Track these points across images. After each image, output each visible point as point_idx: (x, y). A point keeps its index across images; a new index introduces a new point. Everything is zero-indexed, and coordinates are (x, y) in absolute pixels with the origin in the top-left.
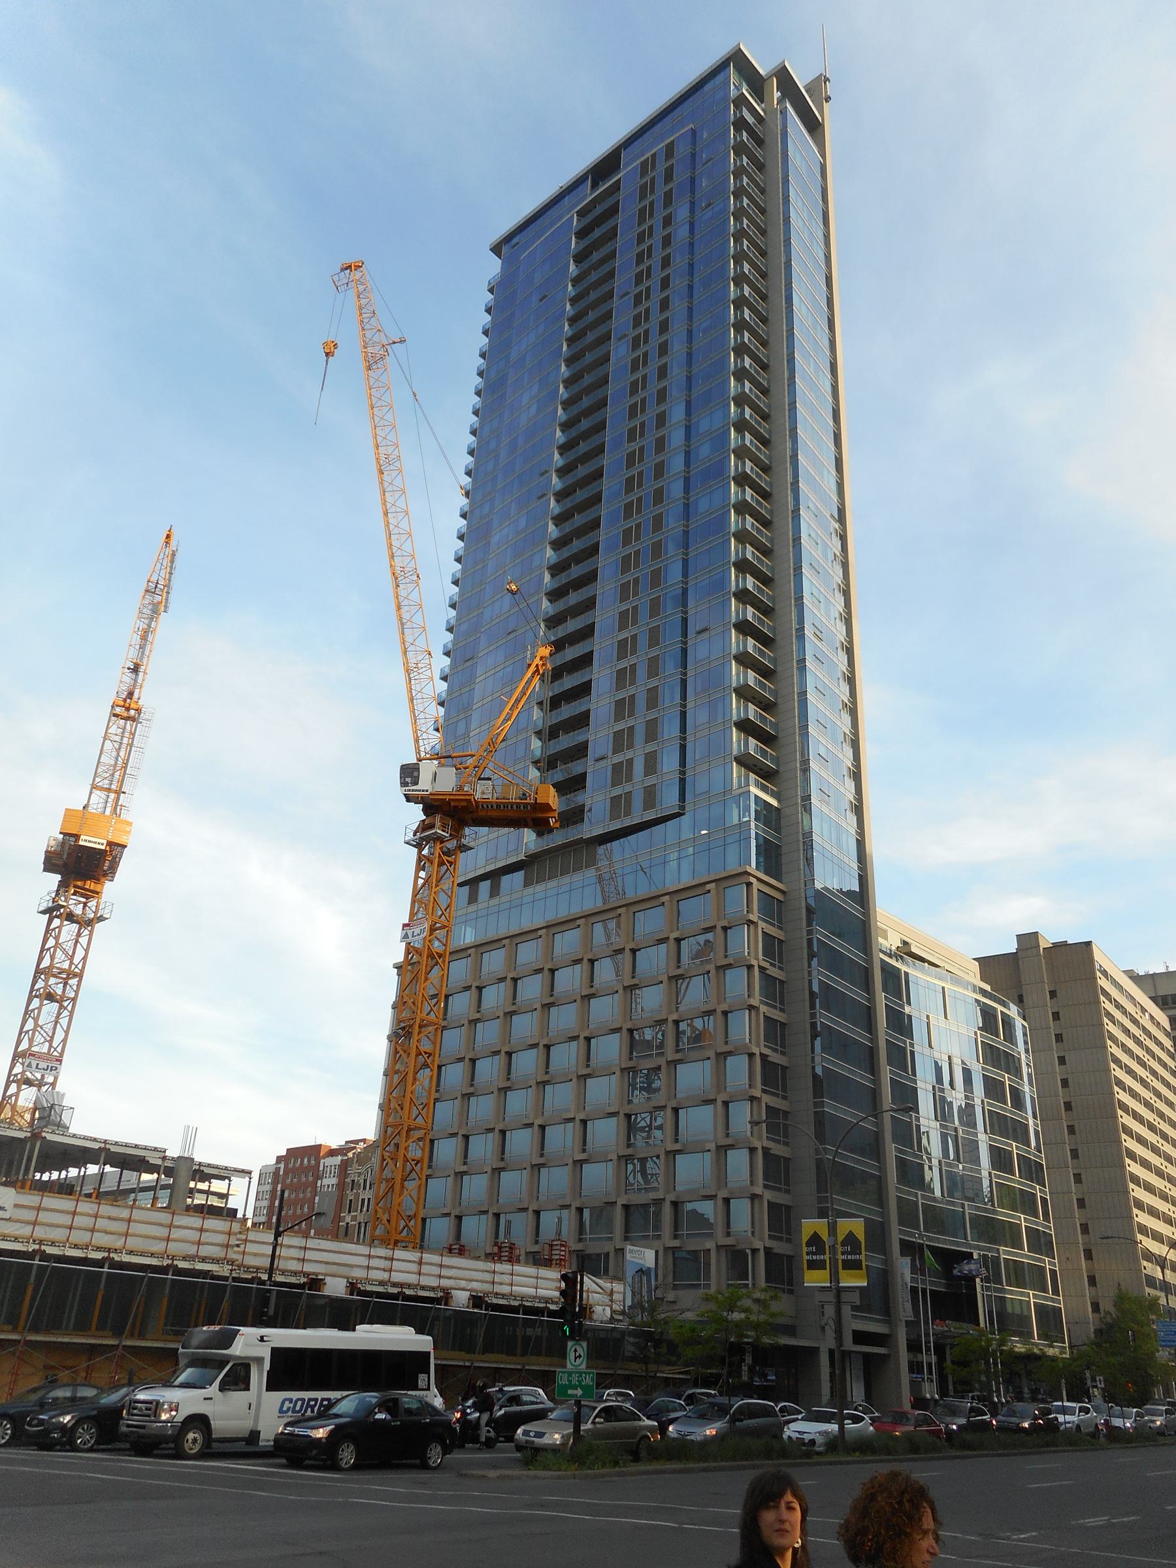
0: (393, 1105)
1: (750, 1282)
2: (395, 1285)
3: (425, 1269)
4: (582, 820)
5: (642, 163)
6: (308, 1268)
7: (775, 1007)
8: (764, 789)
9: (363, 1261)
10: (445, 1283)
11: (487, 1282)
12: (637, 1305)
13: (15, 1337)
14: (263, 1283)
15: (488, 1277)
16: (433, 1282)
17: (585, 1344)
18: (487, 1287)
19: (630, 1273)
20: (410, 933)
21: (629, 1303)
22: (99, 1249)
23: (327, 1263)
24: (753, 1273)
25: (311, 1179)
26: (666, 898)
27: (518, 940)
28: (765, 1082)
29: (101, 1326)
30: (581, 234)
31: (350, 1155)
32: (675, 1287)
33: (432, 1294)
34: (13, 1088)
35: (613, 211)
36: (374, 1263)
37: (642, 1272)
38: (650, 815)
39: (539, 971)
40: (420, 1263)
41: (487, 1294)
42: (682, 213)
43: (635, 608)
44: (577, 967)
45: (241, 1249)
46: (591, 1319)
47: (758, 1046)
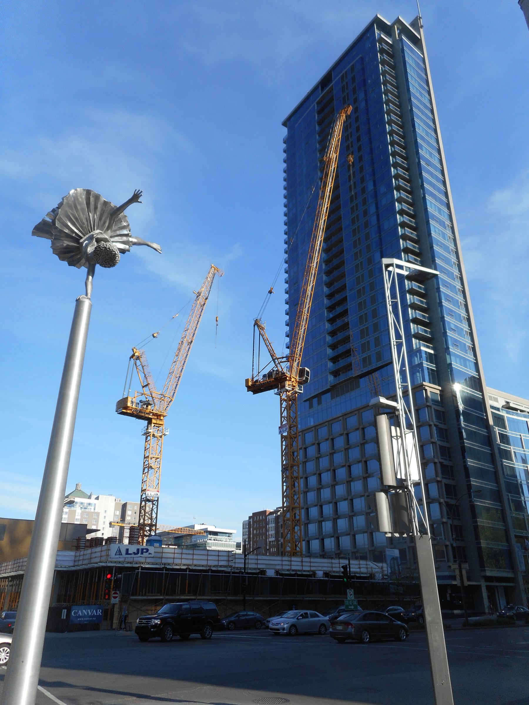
0: (290, 493)
1: (446, 559)
2: (293, 570)
3: (304, 564)
4: (352, 369)
6: (259, 566)
7: (444, 441)
8: (428, 347)
9: (280, 563)
10: (313, 569)
12: (393, 572)
13: (162, 597)
14: (242, 573)
15: (330, 565)
16: (308, 569)
17: (353, 590)
18: (330, 569)
19: (388, 559)
20: (282, 430)
21: (390, 571)
22: (184, 565)
24: (447, 556)
27: (332, 422)
28: (443, 473)
29: (189, 593)
31: (279, 513)
33: (308, 573)
34: (143, 503)
35: (331, 100)
36: (284, 563)
37: (394, 559)
38: (379, 364)
39: (342, 435)
40: (302, 562)
41: (330, 572)
42: (361, 96)
44: (358, 432)
45: (234, 561)
46: (374, 579)
47: (438, 458)
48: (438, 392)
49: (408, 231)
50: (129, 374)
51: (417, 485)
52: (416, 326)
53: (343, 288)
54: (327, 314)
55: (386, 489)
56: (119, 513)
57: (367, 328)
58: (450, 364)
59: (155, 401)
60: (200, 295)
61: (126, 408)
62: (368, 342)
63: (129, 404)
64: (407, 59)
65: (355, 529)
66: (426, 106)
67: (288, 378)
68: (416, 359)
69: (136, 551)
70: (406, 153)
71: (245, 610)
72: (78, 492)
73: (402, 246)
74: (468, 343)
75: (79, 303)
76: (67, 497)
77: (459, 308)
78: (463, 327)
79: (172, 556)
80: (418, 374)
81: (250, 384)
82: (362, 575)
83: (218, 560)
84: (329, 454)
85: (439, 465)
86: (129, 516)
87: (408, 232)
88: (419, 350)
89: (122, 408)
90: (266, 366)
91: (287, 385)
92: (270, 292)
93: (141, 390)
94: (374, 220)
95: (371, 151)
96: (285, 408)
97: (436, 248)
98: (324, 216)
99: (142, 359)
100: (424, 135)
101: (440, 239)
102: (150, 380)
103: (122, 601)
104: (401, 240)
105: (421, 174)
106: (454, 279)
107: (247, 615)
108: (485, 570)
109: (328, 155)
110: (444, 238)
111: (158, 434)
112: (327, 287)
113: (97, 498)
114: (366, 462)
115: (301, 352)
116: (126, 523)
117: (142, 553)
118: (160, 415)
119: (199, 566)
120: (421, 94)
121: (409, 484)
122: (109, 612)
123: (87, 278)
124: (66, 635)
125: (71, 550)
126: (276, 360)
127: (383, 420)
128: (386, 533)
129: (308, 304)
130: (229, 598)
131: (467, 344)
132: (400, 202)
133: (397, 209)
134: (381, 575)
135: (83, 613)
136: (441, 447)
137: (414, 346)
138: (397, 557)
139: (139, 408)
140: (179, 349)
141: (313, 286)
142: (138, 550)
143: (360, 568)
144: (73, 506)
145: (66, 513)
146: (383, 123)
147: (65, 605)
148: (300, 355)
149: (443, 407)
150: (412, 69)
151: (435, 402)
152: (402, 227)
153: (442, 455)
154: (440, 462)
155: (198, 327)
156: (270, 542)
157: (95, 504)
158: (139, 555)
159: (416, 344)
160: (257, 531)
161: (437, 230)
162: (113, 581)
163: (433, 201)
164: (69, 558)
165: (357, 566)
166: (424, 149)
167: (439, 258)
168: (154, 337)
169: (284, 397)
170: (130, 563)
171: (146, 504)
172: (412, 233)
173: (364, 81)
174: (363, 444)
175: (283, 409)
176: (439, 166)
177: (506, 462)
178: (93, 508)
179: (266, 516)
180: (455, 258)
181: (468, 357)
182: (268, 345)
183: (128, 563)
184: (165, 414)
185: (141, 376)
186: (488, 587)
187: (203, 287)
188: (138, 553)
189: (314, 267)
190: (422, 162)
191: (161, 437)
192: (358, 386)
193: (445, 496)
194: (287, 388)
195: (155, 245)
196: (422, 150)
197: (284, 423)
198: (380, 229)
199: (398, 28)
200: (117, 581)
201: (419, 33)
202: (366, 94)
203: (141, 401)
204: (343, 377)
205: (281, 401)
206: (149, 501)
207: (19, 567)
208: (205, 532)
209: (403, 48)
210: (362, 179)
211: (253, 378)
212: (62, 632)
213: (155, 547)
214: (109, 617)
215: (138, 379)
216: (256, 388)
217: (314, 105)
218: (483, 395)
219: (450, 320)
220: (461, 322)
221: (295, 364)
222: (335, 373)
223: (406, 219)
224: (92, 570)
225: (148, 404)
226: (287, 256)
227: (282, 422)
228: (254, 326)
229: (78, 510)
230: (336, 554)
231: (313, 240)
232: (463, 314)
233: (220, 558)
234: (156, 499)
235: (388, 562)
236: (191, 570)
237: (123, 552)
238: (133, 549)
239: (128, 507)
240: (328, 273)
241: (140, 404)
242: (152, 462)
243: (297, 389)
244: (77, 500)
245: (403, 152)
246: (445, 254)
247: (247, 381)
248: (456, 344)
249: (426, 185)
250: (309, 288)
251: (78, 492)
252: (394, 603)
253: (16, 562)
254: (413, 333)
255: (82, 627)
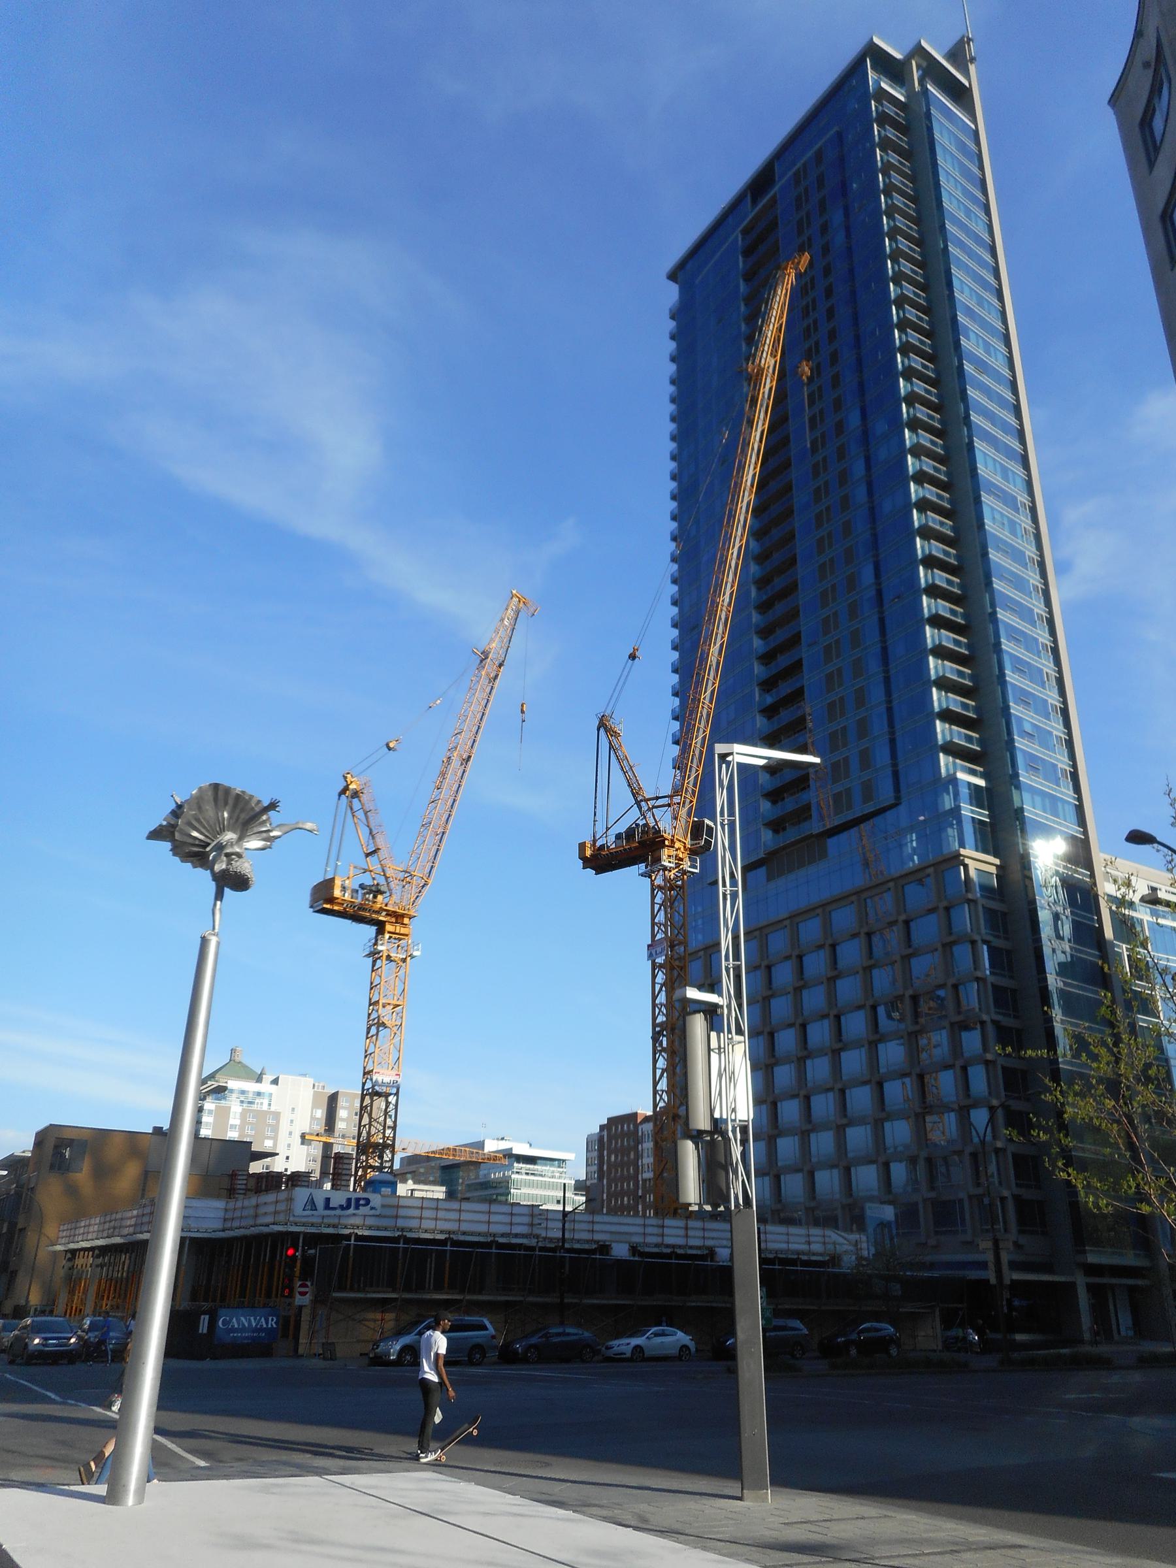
2: (667, 1246)
5: (795, 174)
6: (597, 1237)
8: (973, 772)
9: (641, 1230)
10: (709, 1243)
11: (771, 1233)
13: (394, 1296)
16: (698, 1243)
21: (873, 1250)
22: (442, 1232)
23: (611, 1233)
25: (632, 1143)
26: (891, 884)
30: (748, 252)
32: (937, 1233)
33: (699, 1252)
34: (367, 1100)
35: (773, 225)
36: (649, 1230)
37: (883, 1225)
38: (870, 808)
39: (788, 958)
40: (686, 1228)
42: (837, 218)
43: (835, 614)
44: (822, 952)
47: (988, 1013)
48: (993, 870)
49: (934, 520)
50: (336, 830)
51: (744, 1130)
52: (947, 726)
53: (795, 641)
54: (760, 695)
55: (696, 1136)
56: (320, 1113)
57: (844, 728)
58: (1021, 810)
59: (392, 885)
60: (486, 658)
61: (332, 900)
62: (846, 760)
63: (337, 893)
64: (937, 135)
65: (814, 1160)
66: (978, 240)
67: (667, 843)
68: (946, 797)
69: (344, 1202)
70: (932, 347)
71: (562, 1323)
72: (235, 1067)
73: (919, 552)
74: (1063, 763)
75: (204, 942)
76: (212, 1076)
77: (1044, 687)
78: (1052, 727)
79: (417, 1213)
80: (950, 831)
81: (588, 853)
82: (814, 1258)
83: (511, 1224)
84: (760, 999)
85: (990, 1028)
86: (343, 1120)
87: (934, 520)
88: (953, 780)
89: (323, 898)
90: (622, 816)
91: (664, 857)
92: (633, 657)
93: (362, 862)
94: (860, 494)
95: (858, 341)
96: (661, 905)
97: (994, 555)
98: (747, 493)
99: (364, 797)
100: (972, 304)
101: (1005, 535)
102: (380, 841)
103: (316, 1301)
104: (918, 539)
105: (964, 392)
106: (1033, 624)
107: (564, 1334)
108: (1085, 1252)
109: (757, 361)
110: (1013, 532)
111: (397, 955)
112: (761, 638)
113: (275, 1082)
114: (838, 1018)
115: (695, 785)
116: (336, 1134)
117: (357, 1208)
118: (403, 916)
119: (472, 1234)
120: (968, 212)
121: (730, 1128)
122: (292, 1323)
123: (215, 905)
124: (208, 1364)
125: (218, 1197)
126: (643, 804)
127: (698, 1023)
128: (690, 1204)
129: (711, 683)
130: (531, 1299)
131: (1060, 765)
132: (916, 455)
133: (911, 471)
134: (854, 1257)
135: (241, 1322)
136: (995, 987)
137: (943, 771)
138: (889, 1223)
139: (358, 901)
140: (443, 775)
141: (722, 645)
142: (349, 1200)
143: (809, 1243)
144: (225, 1098)
145: (210, 1112)
146: (883, 280)
147: (206, 1305)
148: (694, 792)
149: (1002, 901)
150: (948, 158)
151: (986, 889)
152: (920, 511)
153: (998, 1003)
154: (993, 1021)
155: (483, 725)
156: (644, 1181)
157: (271, 1095)
158: (351, 1211)
159: (947, 765)
160: (616, 1157)
161: (997, 516)
162: (299, 1262)
163: (991, 451)
164: (214, 1217)
165: (803, 1240)
166: (972, 336)
167: (1001, 578)
168: (389, 749)
169: (659, 881)
170: (334, 1226)
171: (372, 1101)
172: (942, 524)
173: (844, 187)
174: (832, 980)
175: (657, 907)
176: (1006, 372)
177: (1143, 1020)
178: (266, 1102)
179: (636, 1126)
180: (1038, 577)
181: (1062, 793)
182: (628, 772)
183: (329, 1226)
184: (412, 913)
185: (363, 832)
186: (1090, 1288)
187: (492, 640)
188: (348, 1207)
189: (726, 604)
190: (968, 367)
191: (404, 960)
192: (824, 854)
193: (1003, 1093)
194: (666, 864)
195: (309, 826)
196: (968, 339)
197: (658, 937)
198: (873, 513)
199: (918, 67)
200: (307, 1262)
201: (967, 75)
202: (847, 214)
203: (362, 886)
204: (792, 834)
205: (653, 890)
206: (379, 1094)
207: (114, 1228)
208: (505, 1156)
209: (929, 110)
210: (838, 404)
211: (595, 841)
212: (201, 1358)
213: (383, 1196)
214: (291, 1333)
215: (355, 840)
216: (601, 861)
217: (737, 238)
218: (1092, 876)
219: (1022, 712)
220: (1047, 717)
221: (683, 812)
222: (776, 826)
223: (931, 492)
224: (260, 1239)
225: (377, 892)
226: (675, 567)
227: (653, 936)
228: (598, 730)
229: (235, 1108)
230: (806, 1208)
231: (724, 544)
232: (1053, 698)
233: (516, 1220)
234: (394, 1091)
235: (870, 1230)
236: (456, 1243)
237: (320, 1204)
238: (339, 1198)
239: (342, 1102)
240: (764, 607)
241: (361, 892)
242: (385, 1014)
243: (686, 865)
244: (232, 1084)
245: (927, 345)
246: (1015, 568)
247: (582, 846)
248: (1035, 765)
249: (974, 417)
250: (714, 650)
251: (235, 1067)
252: (877, 1316)
253: (108, 1219)
254: (940, 742)
255: (239, 1350)
